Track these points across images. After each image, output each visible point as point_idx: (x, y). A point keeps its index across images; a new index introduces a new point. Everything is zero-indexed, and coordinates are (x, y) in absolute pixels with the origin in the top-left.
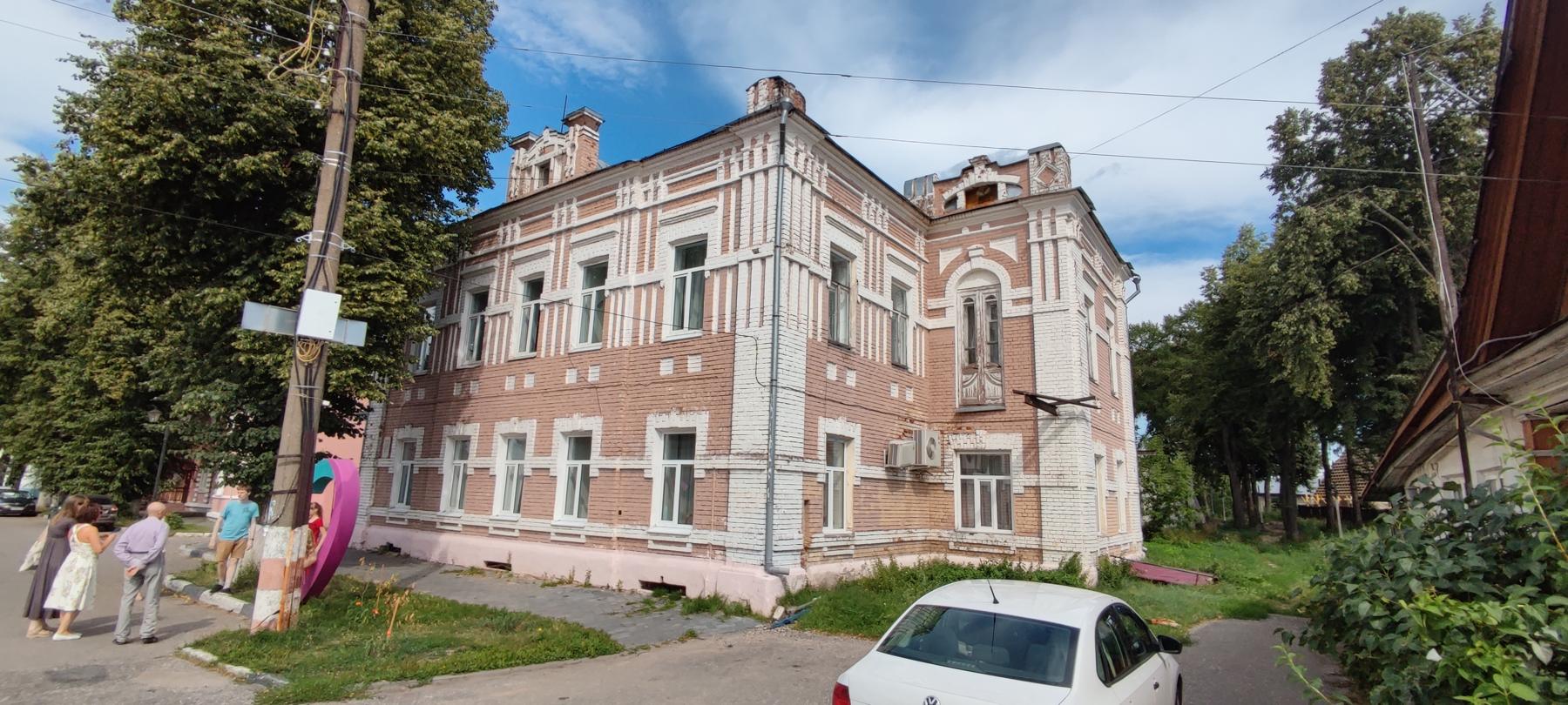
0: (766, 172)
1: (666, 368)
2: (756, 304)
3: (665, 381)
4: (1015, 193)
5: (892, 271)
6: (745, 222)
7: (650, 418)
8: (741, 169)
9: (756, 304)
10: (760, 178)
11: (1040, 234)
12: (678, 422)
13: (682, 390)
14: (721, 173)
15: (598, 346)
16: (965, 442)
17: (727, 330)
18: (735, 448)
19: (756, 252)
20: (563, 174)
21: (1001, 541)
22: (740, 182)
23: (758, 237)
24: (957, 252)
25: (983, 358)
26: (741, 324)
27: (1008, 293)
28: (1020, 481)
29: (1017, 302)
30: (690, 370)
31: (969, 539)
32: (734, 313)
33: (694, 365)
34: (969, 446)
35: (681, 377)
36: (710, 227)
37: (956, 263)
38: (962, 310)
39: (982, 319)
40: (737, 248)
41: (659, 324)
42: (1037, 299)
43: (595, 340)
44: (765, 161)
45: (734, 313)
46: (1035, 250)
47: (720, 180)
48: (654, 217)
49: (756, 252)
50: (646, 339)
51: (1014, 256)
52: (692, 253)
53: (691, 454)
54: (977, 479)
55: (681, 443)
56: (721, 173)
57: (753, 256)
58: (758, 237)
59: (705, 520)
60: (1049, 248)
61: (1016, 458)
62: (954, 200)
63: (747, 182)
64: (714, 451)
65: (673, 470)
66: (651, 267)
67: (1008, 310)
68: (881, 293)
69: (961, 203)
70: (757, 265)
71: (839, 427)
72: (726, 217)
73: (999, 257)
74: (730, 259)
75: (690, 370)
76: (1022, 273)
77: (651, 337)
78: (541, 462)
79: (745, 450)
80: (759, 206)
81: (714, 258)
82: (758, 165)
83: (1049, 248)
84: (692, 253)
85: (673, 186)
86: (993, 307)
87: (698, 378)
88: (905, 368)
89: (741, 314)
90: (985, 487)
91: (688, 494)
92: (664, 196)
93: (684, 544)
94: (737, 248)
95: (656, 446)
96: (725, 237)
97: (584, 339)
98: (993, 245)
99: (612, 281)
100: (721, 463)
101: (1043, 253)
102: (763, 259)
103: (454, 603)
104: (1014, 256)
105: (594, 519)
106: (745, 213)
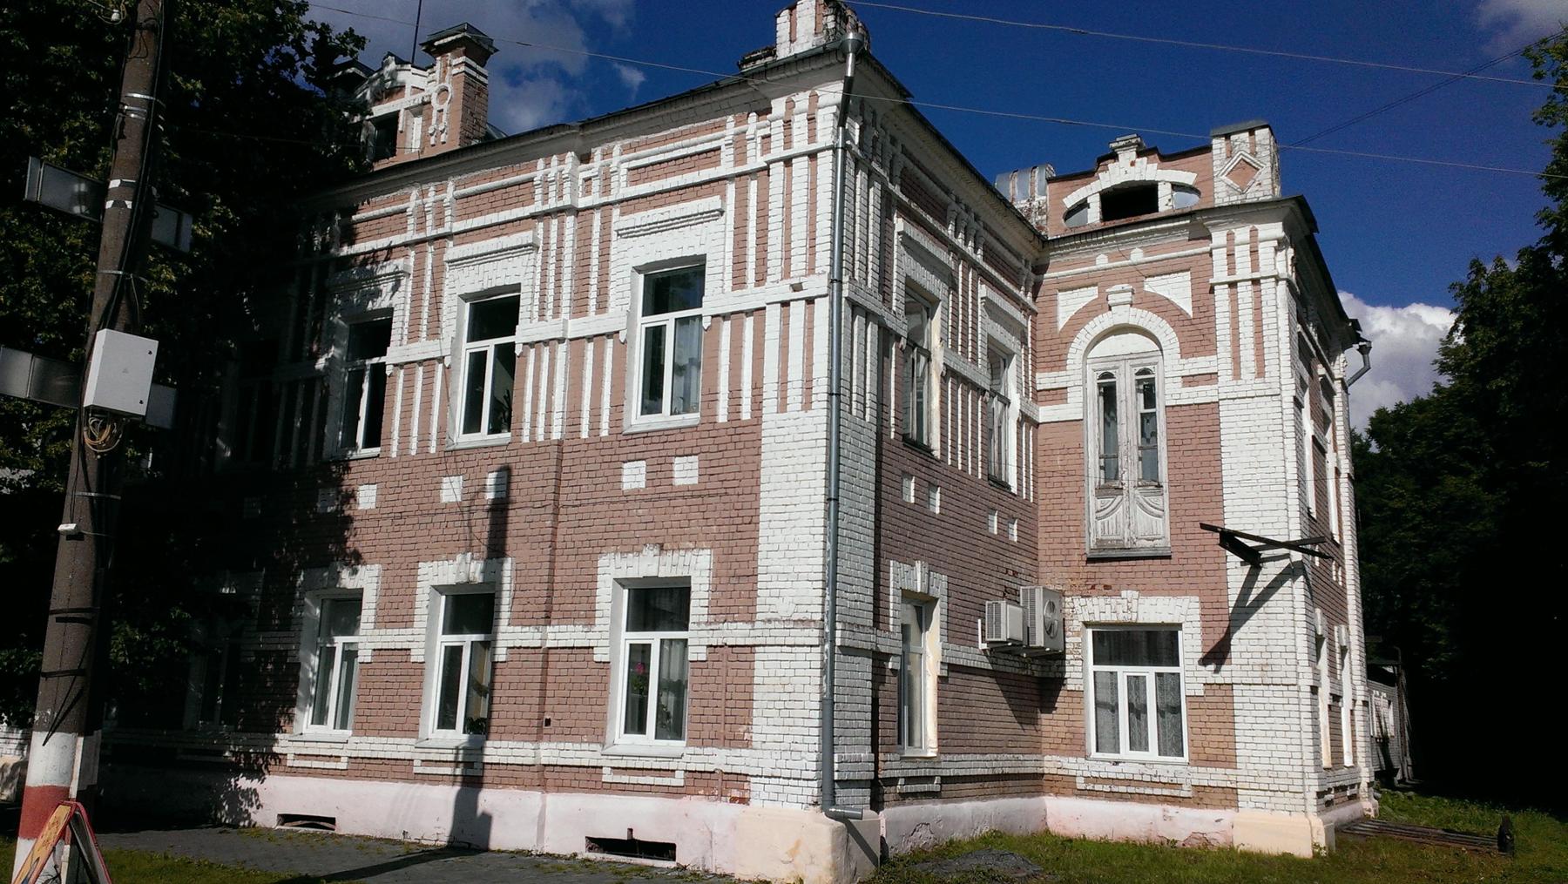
0: (812, 156)
1: (634, 476)
2: (795, 373)
3: (628, 498)
4: (1192, 202)
6: (775, 237)
9: (795, 373)
10: (801, 165)
11: (1232, 269)
12: (649, 565)
13: (663, 516)
14: (727, 155)
17: (746, 415)
18: (762, 611)
19: (797, 288)
20: (425, 137)
21: (1166, 774)
23: (798, 263)
24: (1090, 294)
25: (1130, 471)
26: (770, 405)
28: (1192, 675)
29: (1190, 380)
30: (678, 482)
31: (1112, 771)
32: (757, 387)
33: (685, 472)
35: (660, 488)
36: (710, 242)
37: (1089, 312)
39: (1129, 403)
40: (760, 281)
42: (1225, 378)
44: (812, 138)
45: (757, 387)
46: (1222, 294)
47: (726, 167)
48: (606, 224)
50: (594, 427)
52: (673, 287)
53: (680, 619)
54: (1123, 672)
55: (658, 604)
56: (727, 155)
57: (789, 295)
58: (798, 263)
59: (707, 731)
60: (1245, 291)
62: (1083, 205)
63: (778, 170)
66: (602, 307)
67: (1170, 393)
68: (975, 361)
69: (1093, 215)
71: (916, 577)
73: (1162, 307)
74: (752, 297)
75: (678, 482)
76: (1197, 333)
78: (393, 638)
79: (783, 614)
81: (717, 296)
82: (800, 144)
83: (1245, 291)
86: (1148, 392)
87: (689, 493)
90: (1136, 684)
91: (480, 690)
92: (622, 188)
93: (930, 779)
94: (760, 281)
97: (472, 424)
98: (1154, 286)
99: (527, 330)
100: (736, 633)
101: (1234, 300)
102: (810, 301)
104: (1189, 309)
105: (361, 730)
106: (775, 221)
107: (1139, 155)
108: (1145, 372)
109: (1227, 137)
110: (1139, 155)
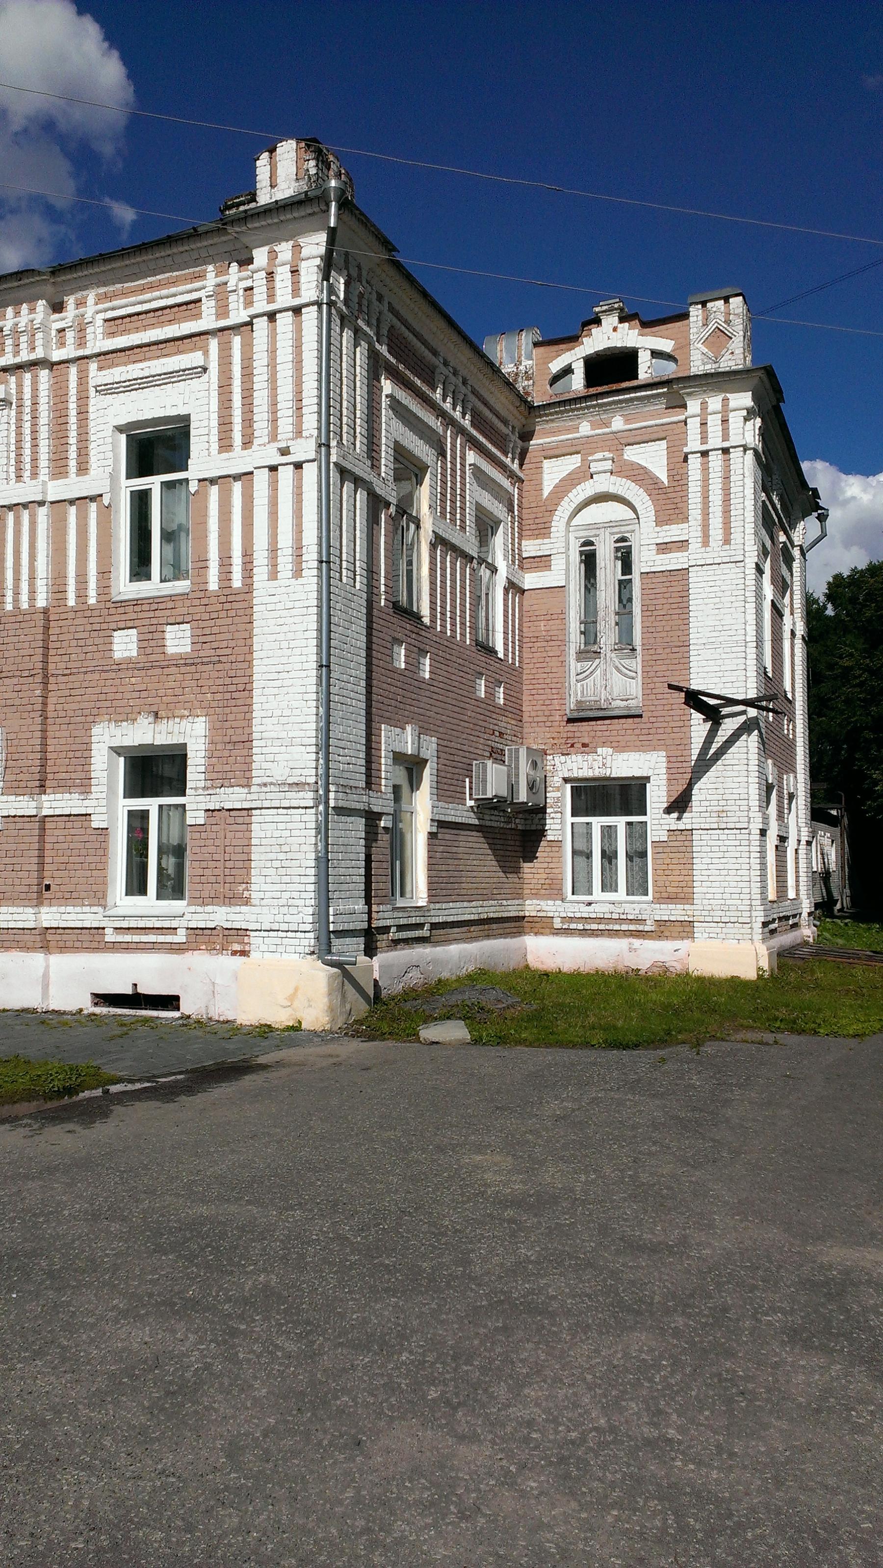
0: (297, 311)
1: (125, 645)
2: (285, 540)
4: (669, 369)
5: (475, 494)
7: (96, 730)
8: (249, 303)
9: (285, 540)
10: (285, 320)
11: (704, 439)
12: (143, 733)
13: (155, 683)
14: (208, 307)
15: (182, 586)
16: (582, 766)
17: (237, 582)
19: (284, 452)
22: (250, 324)
23: (285, 425)
24: (573, 462)
25: (608, 636)
26: (260, 573)
27: (646, 540)
29: (664, 548)
33: (178, 640)
34: (586, 773)
36: (193, 401)
38: (575, 557)
39: (608, 570)
40: (247, 443)
41: (105, 573)
43: (175, 571)
44: (296, 291)
46: (695, 462)
47: (207, 321)
48: (83, 380)
49: (284, 452)
50: (81, 595)
51: (663, 476)
54: (598, 822)
55: (156, 771)
56: (208, 307)
58: (285, 425)
60: (716, 459)
61: (657, 796)
63: (261, 324)
64: (218, 777)
65: (143, 815)
67: (645, 560)
68: (463, 528)
69: (577, 382)
70: (286, 474)
71: (407, 740)
72: (225, 388)
73: (639, 475)
76: (670, 502)
77: (24, 597)
80: (285, 372)
81: (204, 459)
82: (284, 298)
83: (716, 459)
84: (157, 448)
85: (115, 325)
86: (626, 559)
88: (492, 651)
89: (261, 557)
90: (609, 832)
92: (98, 342)
94: (247, 443)
95: (107, 772)
96: (225, 424)
98: (632, 454)
102: (298, 466)
103: (397, 1040)
104: (663, 476)
107: (622, 320)
108: (623, 539)
109: (704, 304)
110: (622, 320)
